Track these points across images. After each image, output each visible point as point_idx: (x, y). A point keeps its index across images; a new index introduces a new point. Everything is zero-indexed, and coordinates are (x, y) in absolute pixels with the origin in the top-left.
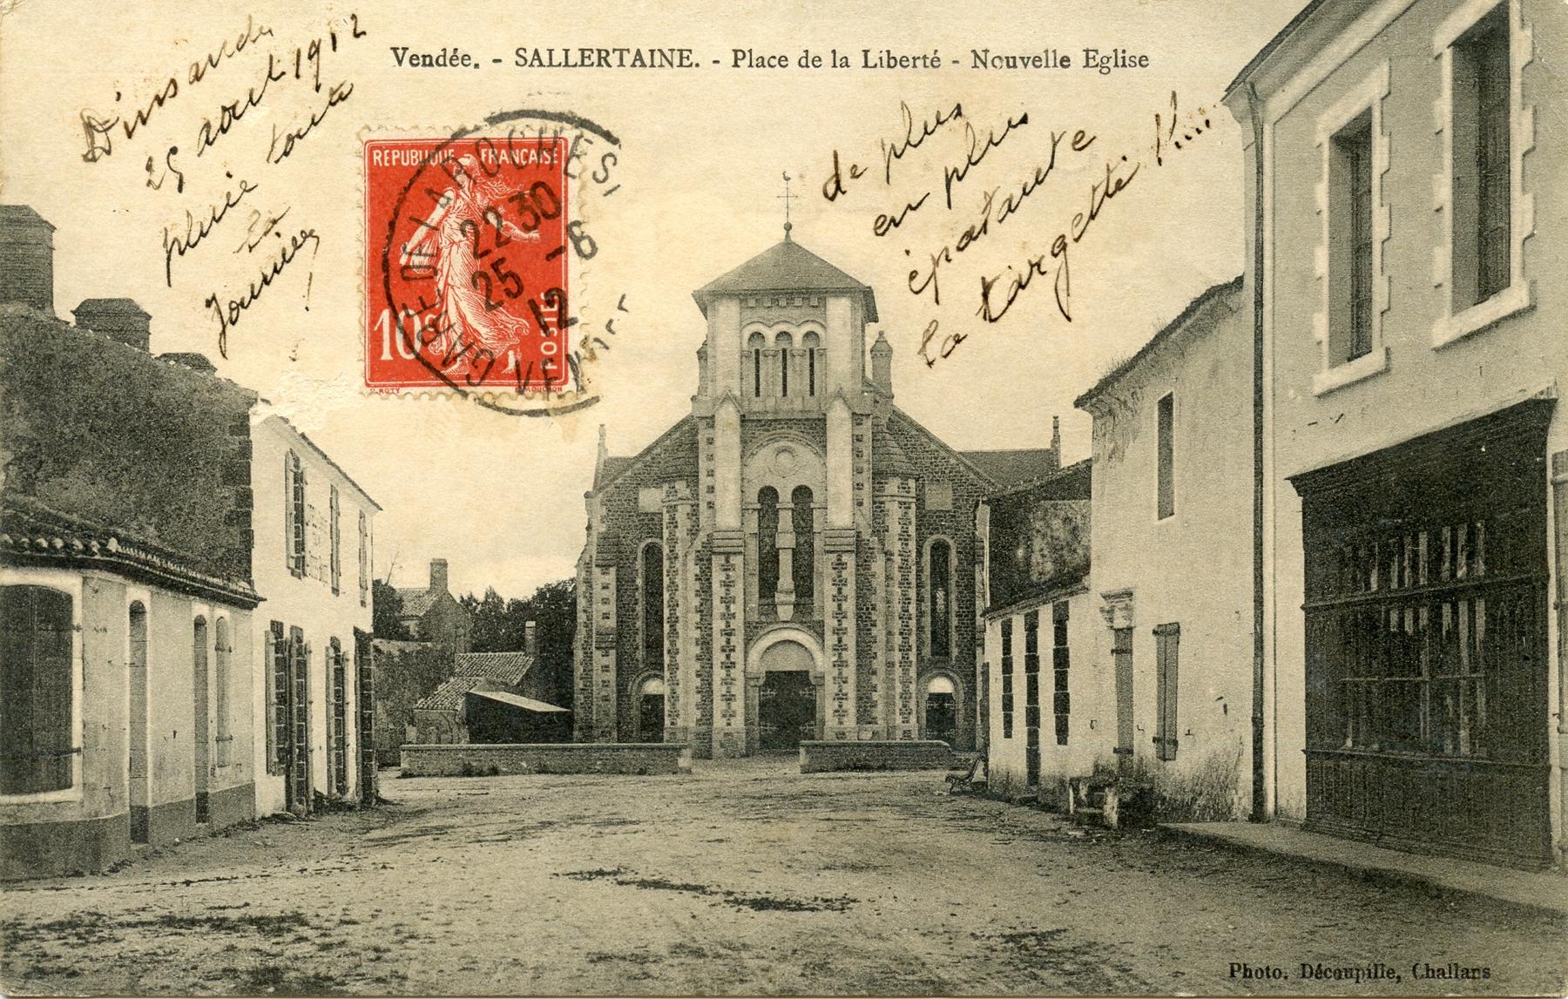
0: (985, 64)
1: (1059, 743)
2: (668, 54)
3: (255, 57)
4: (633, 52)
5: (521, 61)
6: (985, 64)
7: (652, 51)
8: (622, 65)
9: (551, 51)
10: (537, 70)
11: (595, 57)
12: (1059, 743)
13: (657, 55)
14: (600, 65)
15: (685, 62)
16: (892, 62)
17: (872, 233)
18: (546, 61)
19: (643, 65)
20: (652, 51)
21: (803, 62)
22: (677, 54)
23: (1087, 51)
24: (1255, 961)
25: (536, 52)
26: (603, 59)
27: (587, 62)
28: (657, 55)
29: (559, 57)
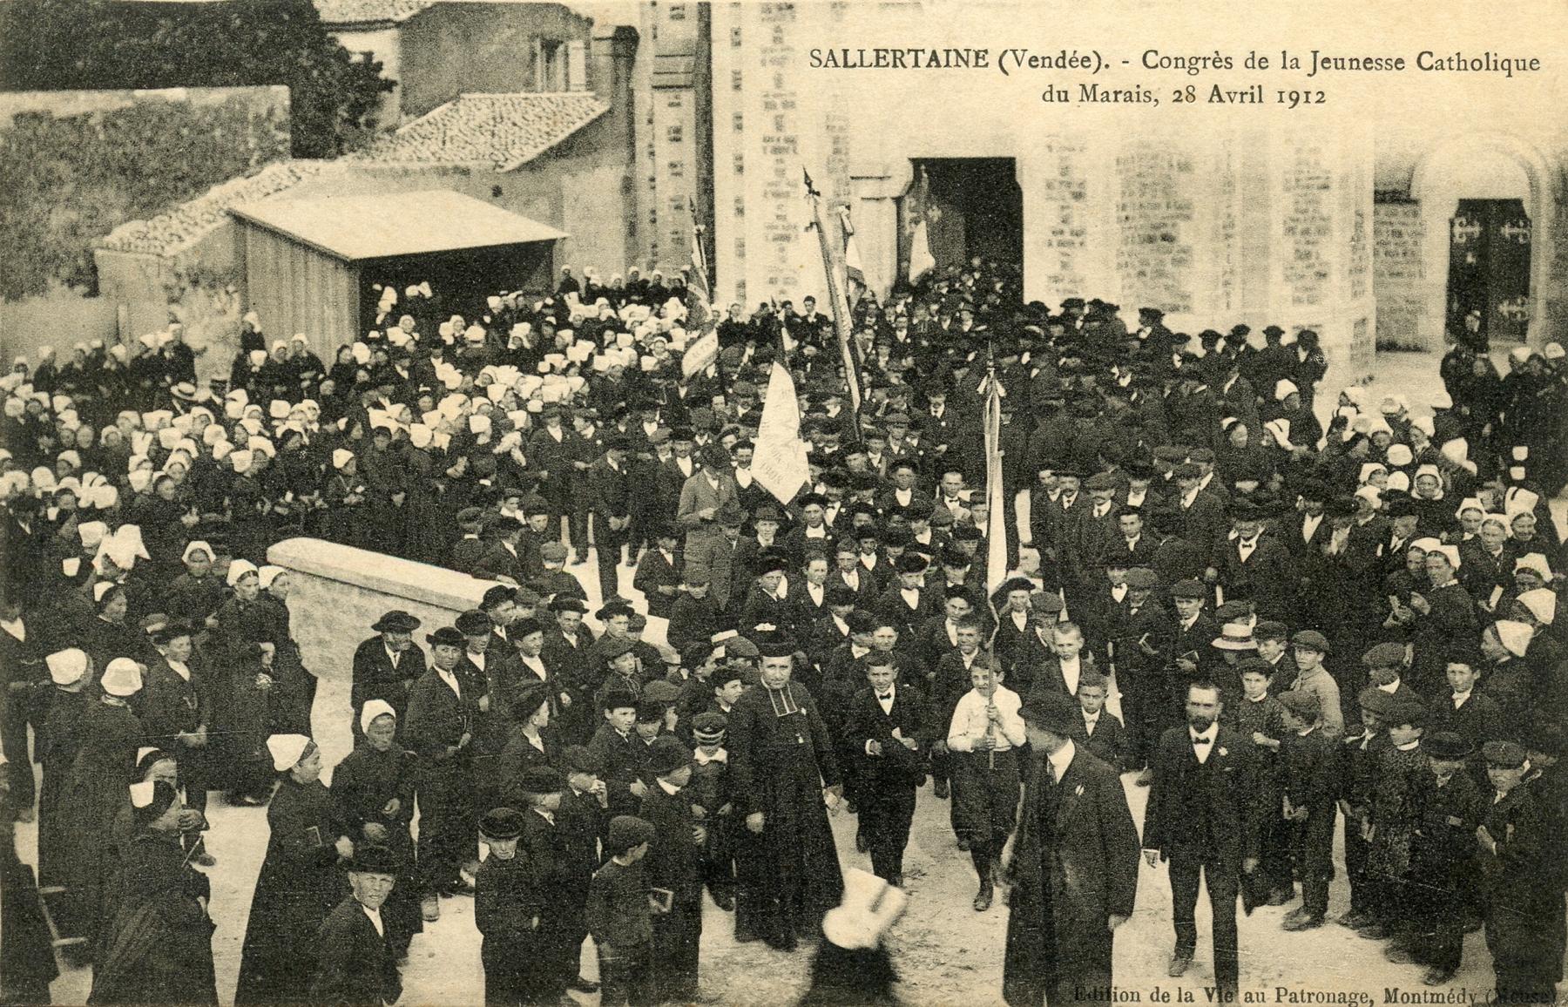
0: (966, 63)
1: (708, 4)
2: (964, 54)
3: (1087, 76)
4: (928, 55)
5: (816, 62)
6: (966, 63)
7: (948, 51)
8: (916, 65)
9: (845, 51)
10: (831, 69)
11: (890, 57)
12: (708, 4)
13: (953, 55)
14: (895, 66)
15: (981, 62)
16: (1506, 65)
17: (972, 910)
18: (841, 62)
19: (938, 65)
20: (948, 51)
21: (1250, 63)
22: (972, 54)
23: (877, 51)
24: (659, 32)
25: (934, 52)
26: (898, 59)
27: (882, 62)
28: (953, 55)
29: (853, 57)
